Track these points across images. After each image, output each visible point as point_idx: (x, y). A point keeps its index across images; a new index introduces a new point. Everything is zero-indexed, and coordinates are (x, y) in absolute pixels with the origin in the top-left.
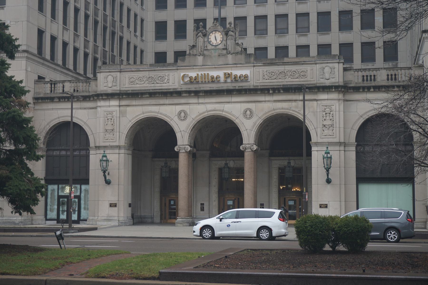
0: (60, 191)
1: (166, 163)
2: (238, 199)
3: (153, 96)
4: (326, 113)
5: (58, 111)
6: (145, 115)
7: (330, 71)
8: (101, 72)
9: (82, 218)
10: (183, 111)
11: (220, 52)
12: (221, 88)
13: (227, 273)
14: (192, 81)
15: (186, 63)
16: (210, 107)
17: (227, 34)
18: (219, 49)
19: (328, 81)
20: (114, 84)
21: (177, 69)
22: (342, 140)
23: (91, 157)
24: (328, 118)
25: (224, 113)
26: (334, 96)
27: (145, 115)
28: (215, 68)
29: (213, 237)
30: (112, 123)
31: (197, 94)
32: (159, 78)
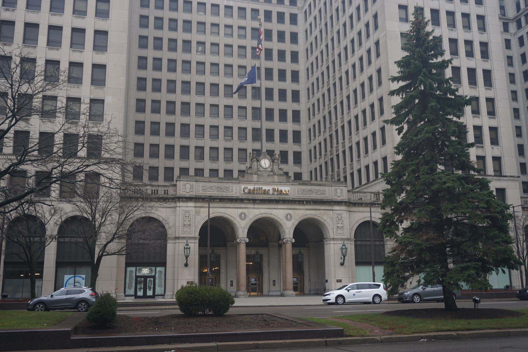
0: (137, 272)
1: (213, 251)
2: (259, 277)
3: (222, 201)
5: (239, 210)
6: (215, 214)
7: (340, 192)
8: (180, 181)
9: (156, 294)
10: (244, 213)
11: (269, 173)
12: (270, 198)
13: (76, 338)
14: (250, 192)
15: (246, 178)
16: (263, 211)
17: (273, 161)
18: (267, 171)
19: (340, 198)
20: (191, 190)
21: (239, 183)
22: (349, 237)
23: (168, 245)
24: (340, 222)
25: (272, 216)
26: (343, 208)
27: (215, 214)
28: (266, 184)
29: (344, 303)
30: (189, 219)
31: (254, 201)
32: (225, 188)
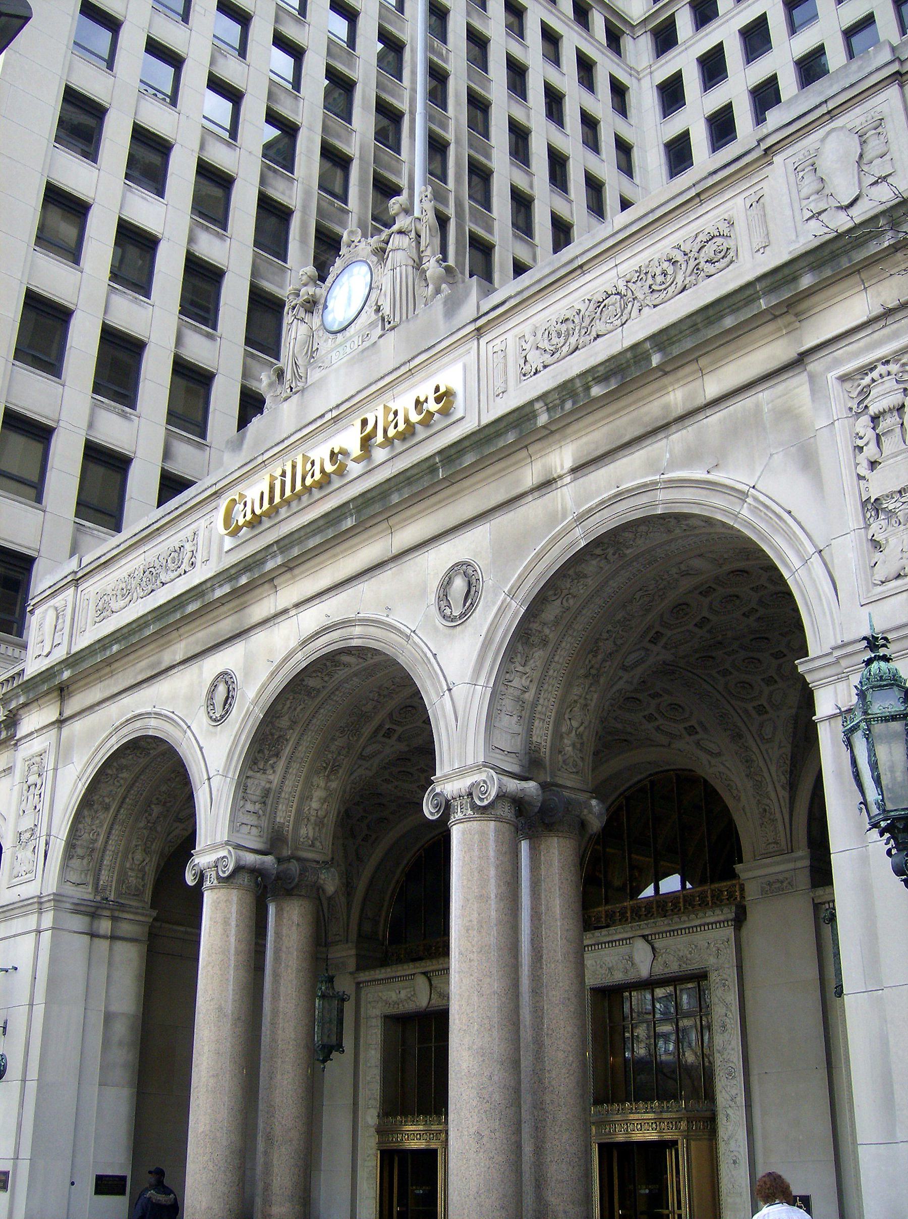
4: (875, 419)
